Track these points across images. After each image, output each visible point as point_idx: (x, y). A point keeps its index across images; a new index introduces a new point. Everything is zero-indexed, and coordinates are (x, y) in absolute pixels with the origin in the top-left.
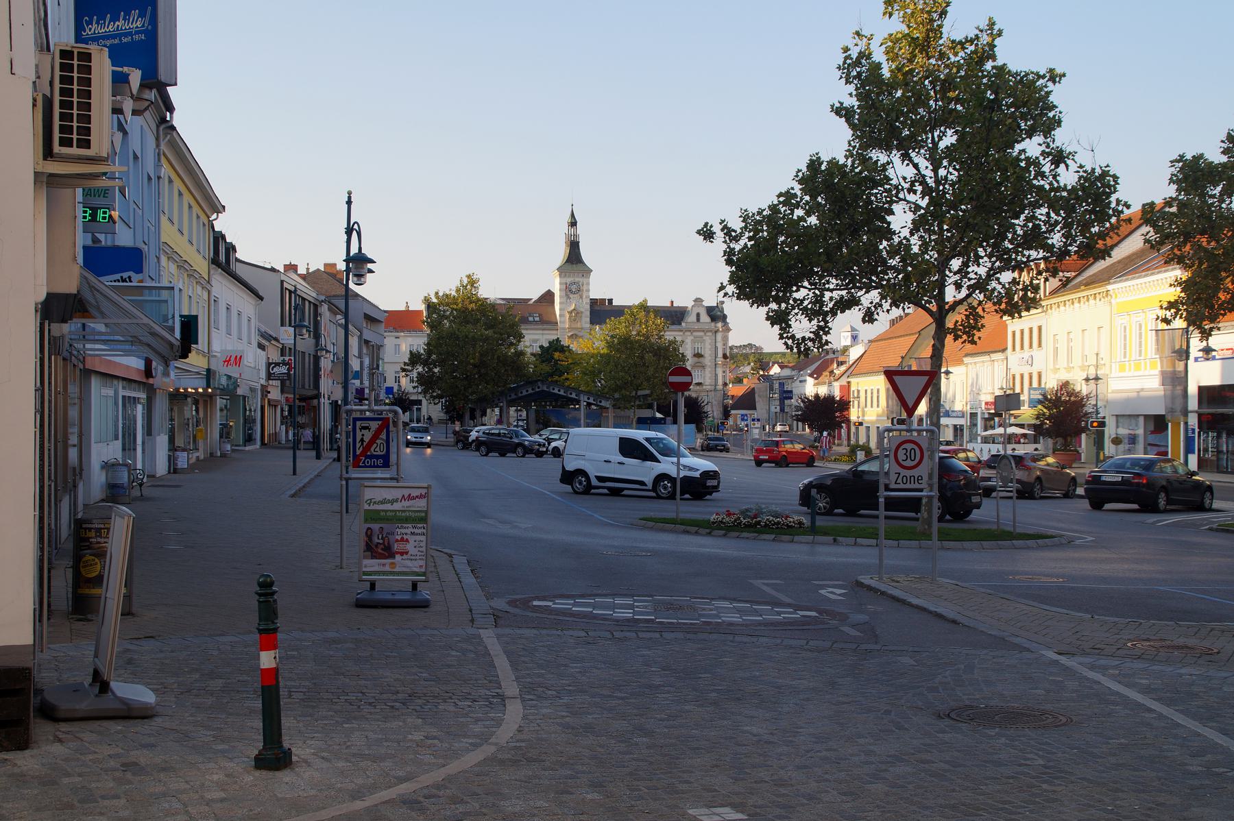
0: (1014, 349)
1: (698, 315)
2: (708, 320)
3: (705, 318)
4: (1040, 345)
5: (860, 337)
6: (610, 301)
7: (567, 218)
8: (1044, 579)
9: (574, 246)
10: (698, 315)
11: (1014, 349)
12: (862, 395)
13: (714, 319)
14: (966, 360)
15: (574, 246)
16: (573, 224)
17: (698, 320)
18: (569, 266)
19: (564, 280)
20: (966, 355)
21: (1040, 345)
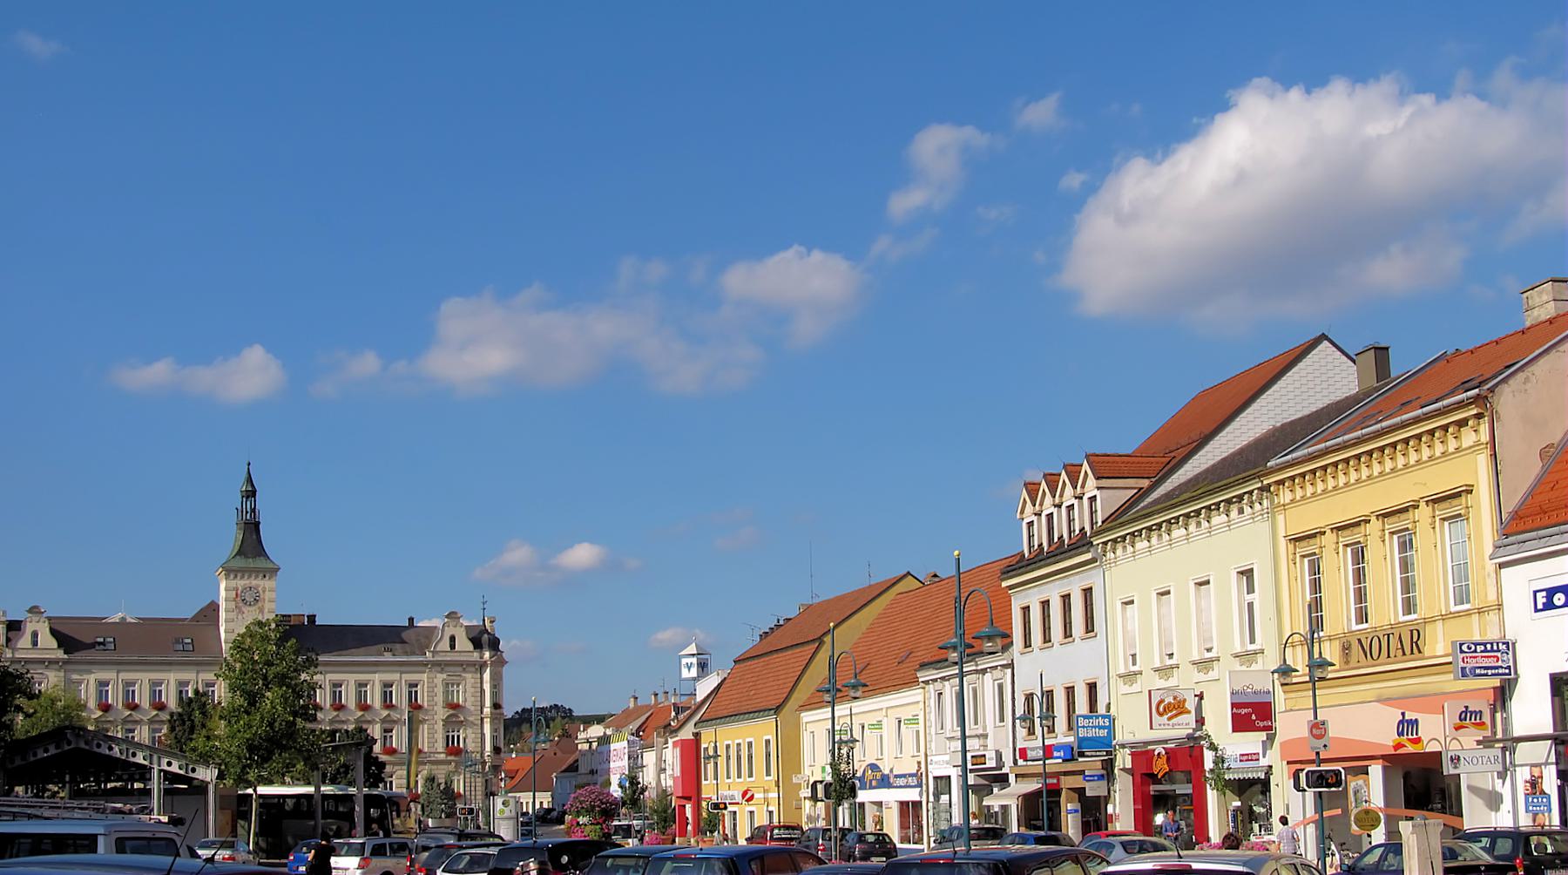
0: (1027, 643)
1: (453, 639)
2: (470, 647)
3: (463, 644)
4: (1089, 626)
5: (712, 664)
6: (312, 618)
7: (241, 485)
8: (388, 657)
9: (251, 527)
10: (453, 639)
11: (1027, 643)
12: (722, 751)
13: (477, 644)
14: (923, 676)
15: (251, 527)
16: (251, 494)
17: (453, 646)
18: (240, 562)
19: (233, 583)
20: (923, 666)
21: (1089, 626)
